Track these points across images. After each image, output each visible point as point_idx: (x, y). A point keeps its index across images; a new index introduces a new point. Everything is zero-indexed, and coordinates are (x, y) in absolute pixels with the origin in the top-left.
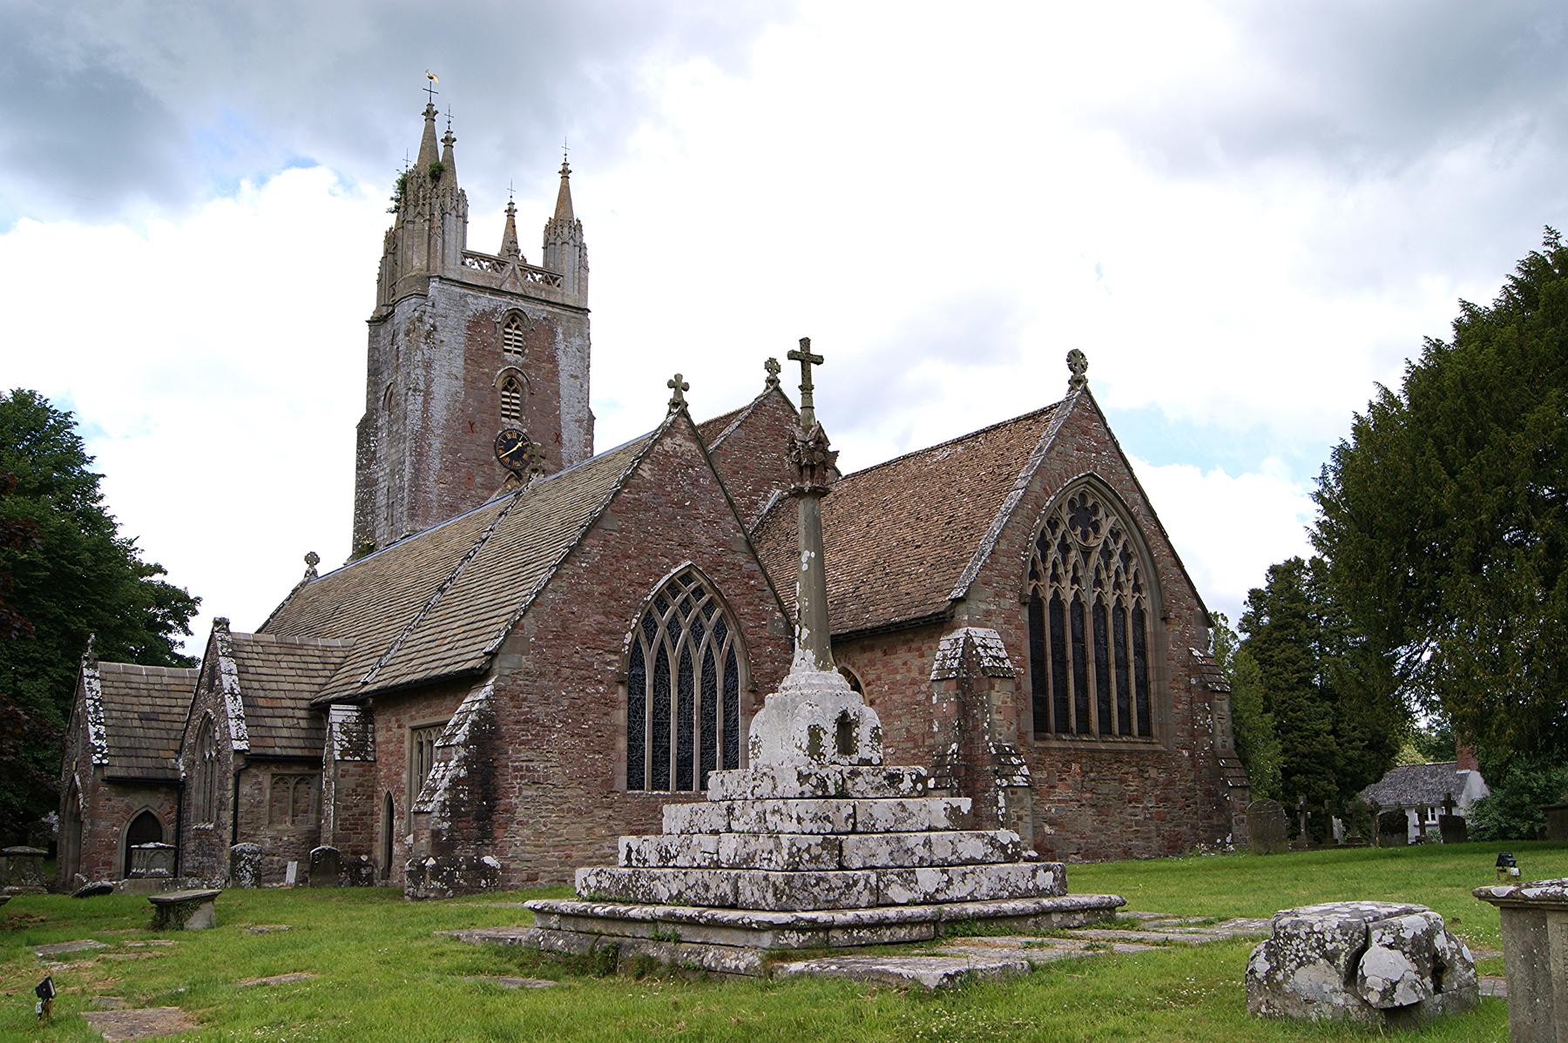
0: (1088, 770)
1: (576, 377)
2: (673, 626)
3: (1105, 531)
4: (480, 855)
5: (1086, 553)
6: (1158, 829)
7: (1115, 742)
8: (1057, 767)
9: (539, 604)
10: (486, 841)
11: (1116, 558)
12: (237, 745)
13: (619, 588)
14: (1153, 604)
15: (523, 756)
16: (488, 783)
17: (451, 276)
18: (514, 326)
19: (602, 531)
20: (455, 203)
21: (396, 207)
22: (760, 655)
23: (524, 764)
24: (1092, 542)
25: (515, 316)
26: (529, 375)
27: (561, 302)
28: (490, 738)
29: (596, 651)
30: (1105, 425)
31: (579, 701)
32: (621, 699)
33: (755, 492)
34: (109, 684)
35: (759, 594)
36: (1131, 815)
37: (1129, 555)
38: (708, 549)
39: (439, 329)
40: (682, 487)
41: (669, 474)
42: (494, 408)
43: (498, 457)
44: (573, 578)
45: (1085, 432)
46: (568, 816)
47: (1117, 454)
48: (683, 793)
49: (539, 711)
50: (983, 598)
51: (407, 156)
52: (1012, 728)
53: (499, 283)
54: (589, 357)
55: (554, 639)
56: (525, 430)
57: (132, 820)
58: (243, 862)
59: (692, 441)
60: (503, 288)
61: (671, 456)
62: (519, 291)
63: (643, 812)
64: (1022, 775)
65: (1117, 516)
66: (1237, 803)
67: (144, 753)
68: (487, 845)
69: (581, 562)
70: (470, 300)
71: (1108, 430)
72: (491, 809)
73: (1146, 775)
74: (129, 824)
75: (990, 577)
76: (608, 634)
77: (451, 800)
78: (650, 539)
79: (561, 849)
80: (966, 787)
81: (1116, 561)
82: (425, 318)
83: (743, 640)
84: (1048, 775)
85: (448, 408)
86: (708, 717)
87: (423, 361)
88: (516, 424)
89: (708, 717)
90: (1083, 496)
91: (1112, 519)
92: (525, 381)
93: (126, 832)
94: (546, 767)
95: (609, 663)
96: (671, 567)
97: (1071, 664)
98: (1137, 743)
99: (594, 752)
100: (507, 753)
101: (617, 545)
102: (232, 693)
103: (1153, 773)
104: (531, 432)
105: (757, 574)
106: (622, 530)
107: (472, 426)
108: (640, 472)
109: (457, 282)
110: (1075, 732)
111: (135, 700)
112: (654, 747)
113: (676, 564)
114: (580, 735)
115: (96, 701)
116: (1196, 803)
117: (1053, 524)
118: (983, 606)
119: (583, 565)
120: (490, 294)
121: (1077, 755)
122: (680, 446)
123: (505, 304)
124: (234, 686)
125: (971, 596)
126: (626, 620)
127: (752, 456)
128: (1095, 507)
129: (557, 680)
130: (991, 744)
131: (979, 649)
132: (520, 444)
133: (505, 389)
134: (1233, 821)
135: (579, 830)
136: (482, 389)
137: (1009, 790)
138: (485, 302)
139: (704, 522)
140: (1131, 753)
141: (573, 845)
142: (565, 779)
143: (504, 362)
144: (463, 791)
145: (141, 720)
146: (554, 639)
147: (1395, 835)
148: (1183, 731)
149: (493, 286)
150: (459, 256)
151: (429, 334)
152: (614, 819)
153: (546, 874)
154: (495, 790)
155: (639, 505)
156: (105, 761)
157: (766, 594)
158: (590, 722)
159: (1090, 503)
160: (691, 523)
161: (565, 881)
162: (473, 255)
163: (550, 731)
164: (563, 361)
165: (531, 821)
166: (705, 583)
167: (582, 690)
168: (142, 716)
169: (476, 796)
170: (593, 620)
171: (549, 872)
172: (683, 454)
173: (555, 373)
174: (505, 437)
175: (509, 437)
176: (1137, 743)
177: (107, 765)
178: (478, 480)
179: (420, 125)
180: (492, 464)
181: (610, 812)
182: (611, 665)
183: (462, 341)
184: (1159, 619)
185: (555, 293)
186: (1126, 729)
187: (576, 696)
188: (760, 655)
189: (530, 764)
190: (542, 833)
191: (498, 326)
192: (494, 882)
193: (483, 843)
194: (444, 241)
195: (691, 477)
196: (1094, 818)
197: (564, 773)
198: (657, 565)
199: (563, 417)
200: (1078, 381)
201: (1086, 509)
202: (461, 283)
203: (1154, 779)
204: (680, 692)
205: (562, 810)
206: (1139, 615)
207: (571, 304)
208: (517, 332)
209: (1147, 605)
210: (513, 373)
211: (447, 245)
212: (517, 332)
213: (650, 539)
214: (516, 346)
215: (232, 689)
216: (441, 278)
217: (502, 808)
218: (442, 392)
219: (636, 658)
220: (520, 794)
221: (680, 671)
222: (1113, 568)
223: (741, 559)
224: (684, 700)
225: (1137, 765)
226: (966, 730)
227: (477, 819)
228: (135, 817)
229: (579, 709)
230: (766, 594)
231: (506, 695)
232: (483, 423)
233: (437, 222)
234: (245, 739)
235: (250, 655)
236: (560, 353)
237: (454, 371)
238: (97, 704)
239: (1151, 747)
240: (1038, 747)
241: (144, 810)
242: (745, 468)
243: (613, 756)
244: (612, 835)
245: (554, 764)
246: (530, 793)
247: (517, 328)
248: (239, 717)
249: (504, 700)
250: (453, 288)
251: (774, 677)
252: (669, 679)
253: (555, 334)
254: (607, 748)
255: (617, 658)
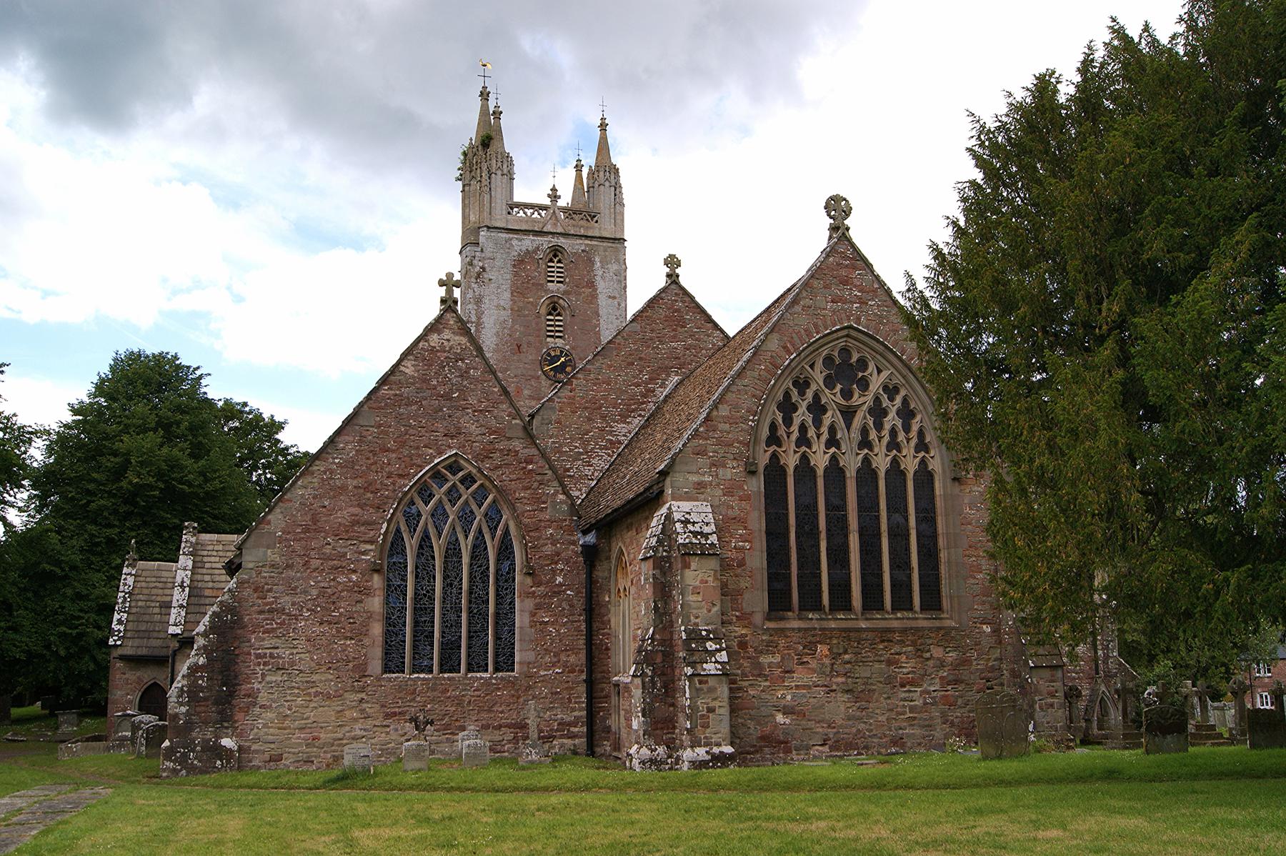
0: (841, 651)
1: (614, 298)
2: (439, 514)
3: (876, 383)
4: (218, 737)
5: (848, 414)
6: (943, 715)
7: (846, 619)
8: (796, 650)
9: (288, 500)
10: (226, 724)
11: (892, 414)
12: (172, 630)
13: (376, 480)
14: (943, 464)
15: (266, 643)
16: (229, 669)
17: (498, 225)
18: (556, 260)
19: (357, 428)
20: (499, 164)
21: (461, 175)
22: (539, 538)
23: (268, 651)
24: (856, 399)
25: (556, 252)
26: (569, 299)
27: (597, 235)
28: (233, 628)
29: (349, 542)
30: (872, 271)
31: (329, 590)
32: (376, 586)
33: (651, 380)
34: (142, 579)
35: (539, 478)
36: (905, 700)
37: (912, 411)
38: (479, 437)
39: (487, 269)
40: (450, 380)
41: (435, 368)
42: (539, 330)
43: (543, 372)
44: (325, 474)
45: (845, 282)
46: (315, 699)
47: (890, 302)
48: (446, 675)
49: (286, 601)
50: (694, 469)
51: (469, 132)
52: (715, 609)
53: (541, 226)
54: (625, 279)
55: (304, 532)
56: (567, 347)
57: (142, 690)
58: (141, 732)
59: (461, 335)
60: (545, 230)
61: (438, 351)
62: (560, 230)
63: (399, 695)
64: (717, 662)
65: (892, 370)
66: (1043, 686)
67: (155, 635)
68: (227, 728)
69: (334, 458)
70: (514, 242)
71: (877, 277)
72: (231, 694)
73: (928, 655)
74: (140, 693)
75: (706, 446)
76: (363, 525)
77: (189, 686)
78: (411, 431)
79: (309, 731)
80: (663, 674)
81: (892, 419)
82: (475, 262)
83: (519, 524)
84: (783, 658)
85: (497, 334)
86: (478, 600)
87: (474, 297)
88: (560, 342)
89: (478, 600)
90: (845, 351)
91: (885, 374)
92: (566, 305)
93: (138, 700)
94: (292, 654)
95: (364, 553)
96: (435, 457)
97: (823, 536)
98: (917, 619)
99: (346, 638)
100: (249, 641)
101: (375, 440)
102: (182, 586)
103: (937, 652)
104: (573, 348)
105: (536, 459)
106: (380, 426)
107: (519, 347)
108: (402, 368)
109: (503, 229)
110: (827, 609)
111: (160, 592)
112: (415, 631)
113: (440, 454)
114: (330, 623)
115: (126, 593)
116: (1002, 685)
117: (802, 385)
118: (695, 478)
119: (337, 461)
120: (533, 235)
121: (826, 636)
122: (448, 340)
123: (545, 242)
124: (185, 579)
125: (677, 468)
126: (384, 511)
127: (649, 347)
128: (863, 364)
129: (305, 571)
130: (683, 628)
131: (678, 525)
132: (563, 359)
133: (550, 314)
134: (1037, 706)
135: (328, 713)
136: (527, 316)
137: (696, 679)
138: (528, 242)
139: (475, 411)
140: (904, 631)
141: (322, 728)
142: (313, 664)
143: (547, 291)
144: (202, 678)
145: (161, 607)
146: (304, 532)
147: (1168, 737)
148: (983, 603)
149: (536, 229)
150: (504, 207)
151: (478, 276)
152: (367, 702)
153: (291, 755)
154: (236, 676)
155: (399, 400)
156: (119, 643)
157: (546, 478)
158: (342, 610)
159: (855, 357)
160: (459, 413)
161: (312, 762)
162: (519, 205)
163: (297, 619)
164: (601, 285)
165: (274, 705)
166: (474, 471)
167: (333, 580)
168: (162, 604)
169: (216, 682)
170: (344, 513)
171: (294, 753)
172: (451, 348)
173: (594, 297)
174: (549, 355)
175: (553, 354)
176: (917, 619)
177: (120, 645)
178: (526, 392)
179: (478, 102)
180: (538, 378)
181: (363, 695)
182: (367, 555)
183: (508, 277)
184: (949, 480)
185: (593, 228)
186: (901, 602)
187: (326, 585)
188: (539, 538)
189: (276, 651)
190: (287, 716)
191: (540, 261)
192: (231, 763)
193: (223, 726)
194: (491, 196)
195: (460, 370)
196: (849, 705)
197: (312, 659)
198: (419, 456)
199: (602, 333)
200: (839, 232)
201: (851, 364)
202: (507, 229)
203: (938, 659)
204: (445, 577)
205: (309, 694)
206: (925, 477)
207: (608, 236)
208: (558, 265)
209: (935, 465)
210: (556, 299)
211: (493, 200)
212: (558, 265)
213: (411, 431)
214: (558, 277)
215: (183, 582)
216: (488, 228)
217: (243, 693)
218: (492, 321)
219: (396, 545)
220: (263, 679)
221: (445, 557)
222: (887, 427)
223: (517, 445)
224: (451, 585)
225: (914, 644)
226: (665, 613)
227: (216, 703)
228: (145, 687)
229: (329, 598)
230: (546, 478)
231: (250, 587)
232: (529, 344)
233: (485, 182)
234: (181, 624)
235: (210, 553)
236: (598, 278)
237: (502, 303)
238: (127, 596)
239: (937, 624)
240: (768, 629)
241: (152, 682)
242: (641, 359)
243: (366, 641)
244: (365, 718)
245: (300, 651)
246: (274, 679)
247: (559, 261)
248: (181, 606)
249: (247, 592)
250: (500, 234)
251: (556, 558)
252: (434, 566)
253: (592, 263)
254: (360, 634)
255: (373, 547)
